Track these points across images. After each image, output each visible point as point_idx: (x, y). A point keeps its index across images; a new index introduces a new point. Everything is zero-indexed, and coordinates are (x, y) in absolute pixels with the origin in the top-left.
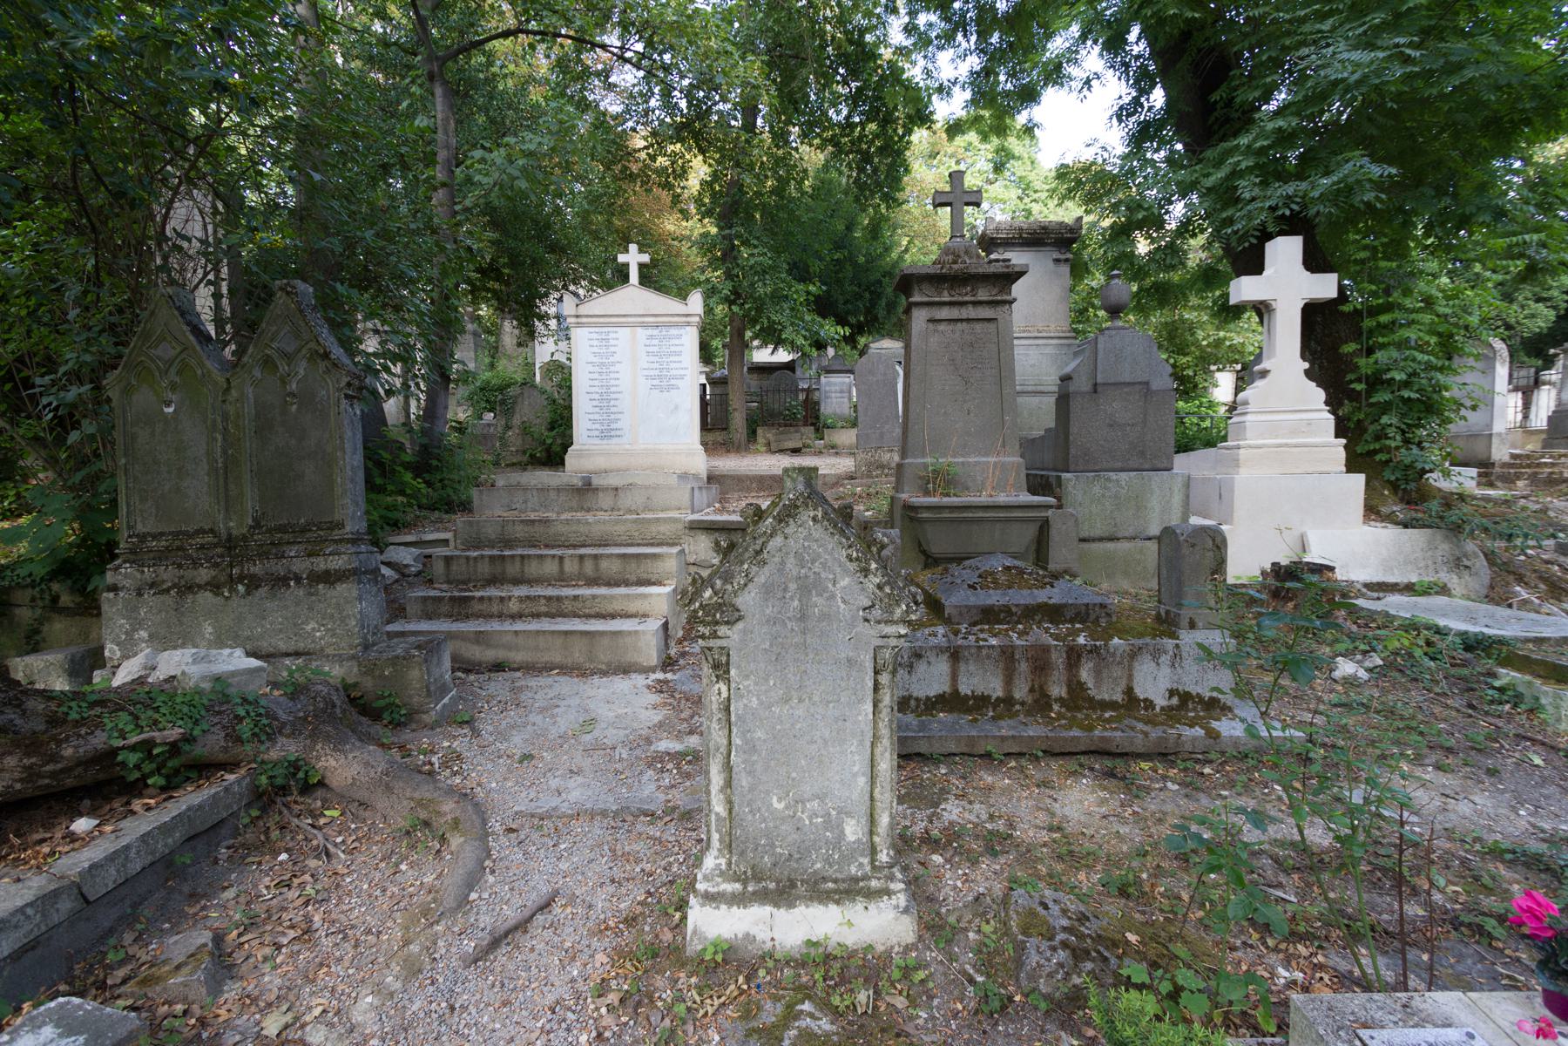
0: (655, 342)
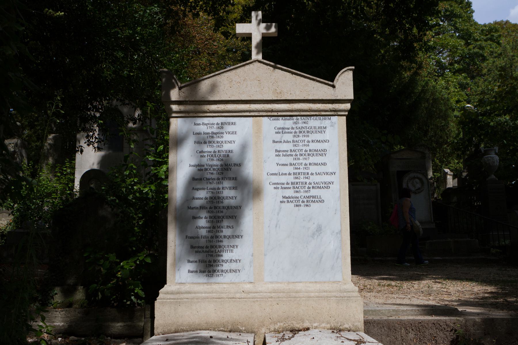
0: (289, 137)
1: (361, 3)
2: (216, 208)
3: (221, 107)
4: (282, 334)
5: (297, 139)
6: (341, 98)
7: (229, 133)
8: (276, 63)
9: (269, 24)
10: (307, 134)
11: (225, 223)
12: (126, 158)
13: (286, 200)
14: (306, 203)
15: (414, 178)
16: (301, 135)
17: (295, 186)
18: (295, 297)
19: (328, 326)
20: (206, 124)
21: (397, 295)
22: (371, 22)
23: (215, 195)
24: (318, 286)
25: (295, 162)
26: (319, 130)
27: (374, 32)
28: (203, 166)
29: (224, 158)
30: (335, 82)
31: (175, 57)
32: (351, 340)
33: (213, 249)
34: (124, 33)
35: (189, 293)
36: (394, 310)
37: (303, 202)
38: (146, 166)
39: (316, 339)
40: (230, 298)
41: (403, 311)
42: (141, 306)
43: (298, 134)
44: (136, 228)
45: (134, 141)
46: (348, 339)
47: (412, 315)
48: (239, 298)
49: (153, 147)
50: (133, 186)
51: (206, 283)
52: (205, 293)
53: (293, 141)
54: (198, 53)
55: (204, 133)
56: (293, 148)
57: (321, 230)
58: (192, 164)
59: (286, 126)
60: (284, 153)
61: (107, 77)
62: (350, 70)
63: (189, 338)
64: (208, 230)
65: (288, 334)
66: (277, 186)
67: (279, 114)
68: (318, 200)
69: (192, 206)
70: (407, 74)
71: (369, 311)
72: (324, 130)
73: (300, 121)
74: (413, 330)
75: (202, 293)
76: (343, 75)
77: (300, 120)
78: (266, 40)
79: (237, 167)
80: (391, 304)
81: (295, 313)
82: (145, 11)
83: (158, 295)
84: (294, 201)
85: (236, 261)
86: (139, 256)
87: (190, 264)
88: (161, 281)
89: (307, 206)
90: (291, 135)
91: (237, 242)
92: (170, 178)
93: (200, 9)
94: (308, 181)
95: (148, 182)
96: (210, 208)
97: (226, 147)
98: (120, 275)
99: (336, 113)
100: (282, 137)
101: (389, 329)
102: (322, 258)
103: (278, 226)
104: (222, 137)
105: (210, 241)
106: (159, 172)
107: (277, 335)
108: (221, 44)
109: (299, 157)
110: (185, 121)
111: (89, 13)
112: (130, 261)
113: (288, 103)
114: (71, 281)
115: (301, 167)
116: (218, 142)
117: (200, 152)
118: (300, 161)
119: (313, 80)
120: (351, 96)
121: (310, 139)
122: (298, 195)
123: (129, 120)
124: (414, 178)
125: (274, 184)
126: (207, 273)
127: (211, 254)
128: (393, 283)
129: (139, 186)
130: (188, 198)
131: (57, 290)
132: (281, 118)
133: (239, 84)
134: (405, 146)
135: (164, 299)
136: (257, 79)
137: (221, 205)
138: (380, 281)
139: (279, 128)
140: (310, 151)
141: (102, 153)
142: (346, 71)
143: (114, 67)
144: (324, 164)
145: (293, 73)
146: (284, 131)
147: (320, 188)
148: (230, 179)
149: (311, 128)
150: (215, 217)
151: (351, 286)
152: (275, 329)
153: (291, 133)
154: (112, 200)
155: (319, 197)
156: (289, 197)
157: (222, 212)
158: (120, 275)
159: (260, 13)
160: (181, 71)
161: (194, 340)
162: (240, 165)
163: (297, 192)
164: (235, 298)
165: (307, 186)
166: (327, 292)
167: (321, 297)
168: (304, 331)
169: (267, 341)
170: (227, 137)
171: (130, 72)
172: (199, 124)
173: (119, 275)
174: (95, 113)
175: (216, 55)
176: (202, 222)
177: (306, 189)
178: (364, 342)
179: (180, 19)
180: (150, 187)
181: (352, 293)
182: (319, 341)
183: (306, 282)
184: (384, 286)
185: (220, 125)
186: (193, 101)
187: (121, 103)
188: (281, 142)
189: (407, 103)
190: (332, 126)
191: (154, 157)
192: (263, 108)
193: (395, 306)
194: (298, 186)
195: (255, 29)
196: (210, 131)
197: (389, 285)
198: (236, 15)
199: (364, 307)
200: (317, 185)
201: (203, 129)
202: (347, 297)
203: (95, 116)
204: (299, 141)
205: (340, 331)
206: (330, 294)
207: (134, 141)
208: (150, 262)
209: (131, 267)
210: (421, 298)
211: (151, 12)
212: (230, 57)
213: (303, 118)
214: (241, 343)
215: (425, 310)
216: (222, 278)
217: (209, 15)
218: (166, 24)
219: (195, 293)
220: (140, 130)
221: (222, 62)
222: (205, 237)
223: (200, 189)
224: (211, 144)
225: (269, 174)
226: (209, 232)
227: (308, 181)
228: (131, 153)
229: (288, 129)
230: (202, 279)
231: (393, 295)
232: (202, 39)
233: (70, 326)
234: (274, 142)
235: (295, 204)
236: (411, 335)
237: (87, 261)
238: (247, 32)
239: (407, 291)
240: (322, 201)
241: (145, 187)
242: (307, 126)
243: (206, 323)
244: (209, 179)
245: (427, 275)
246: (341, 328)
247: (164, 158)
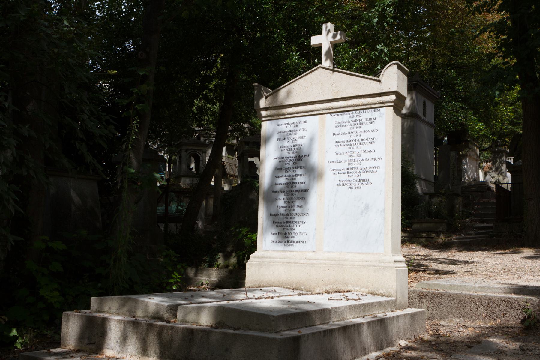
0: (346, 129)
2: (291, 191)
5: (352, 131)
7: (302, 130)
11: (297, 203)
13: (341, 183)
14: (357, 186)
16: (355, 127)
18: (342, 265)
20: (286, 124)
23: (291, 181)
25: (350, 150)
26: (370, 121)
28: (283, 158)
30: (380, 77)
33: (288, 224)
35: (269, 258)
37: (355, 184)
53: (349, 133)
55: (284, 132)
58: (276, 157)
59: (344, 120)
60: (342, 144)
62: (394, 64)
66: (335, 172)
67: (338, 110)
73: (355, 115)
79: (306, 158)
85: (303, 234)
88: (253, 248)
89: (358, 188)
90: (348, 127)
91: (304, 218)
94: (359, 166)
96: (287, 191)
97: (299, 142)
99: (383, 105)
104: (297, 133)
109: (353, 146)
114: (229, 249)
115: (355, 155)
125: (333, 170)
130: (273, 184)
131: (220, 255)
132: (340, 114)
137: (294, 189)
139: (339, 123)
142: (390, 66)
144: (373, 151)
147: (368, 172)
148: (301, 167)
149: (364, 120)
153: (348, 125)
156: (344, 181)
162: (307, 156)
163: (351, 176)
165: (358, 171)
167: (363, 266)
170: (300, 134)
172: (281, 125)
176: (281, 203)
177: (358, 174)
188: (339, 134)
190: (380, 116)
194: (351, 171)
196: (288, 129)
201: (284, 128)
215: (511, 289)
219: (273, 258)
226: (286, 210)
227: (359, 166)
230: (280, 247)
233: (220, 281)
234: (334, 134)
236: (481, 310)
240: (370, 184)
246: (377, 292)
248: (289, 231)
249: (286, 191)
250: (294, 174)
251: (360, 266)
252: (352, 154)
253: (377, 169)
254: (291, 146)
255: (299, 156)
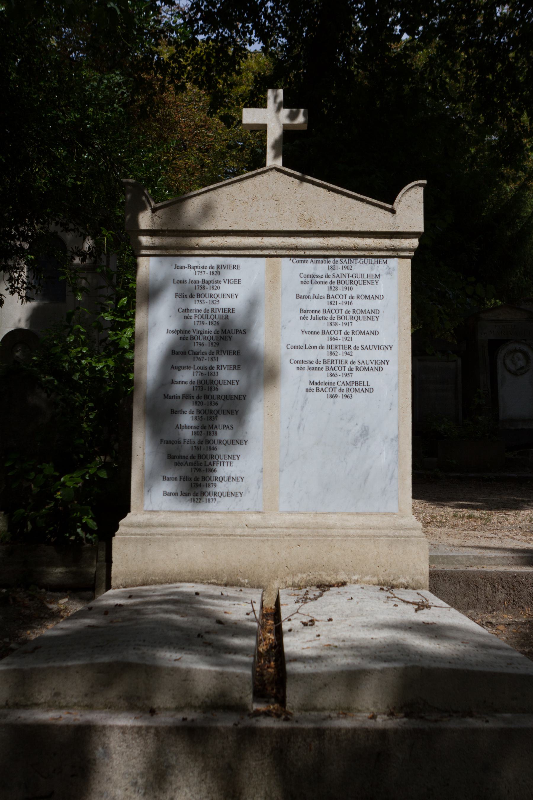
0: (322, 290)
1: (441, 72)
2: (206, 397)
3: (218, 241)
4: (304, 590)
5: (334, 293)
6: (405, 230)
7: (229, 281)
8: (304, 172)
9: (294, 110)
10: (350, 286)
11: (222, 420)
12: (69, 316)
13: (314, 387)
14: (345, 393)
15: (516, 351)
16: (340, 286)
17: (330, 366)
18: (325, 536)
19: (375, 580)
20: (194, 268)
21: (482, 533)
22: (455, 102)
24: (361, 520)
25: (330, 328)
27: (460, 120)
28: (188, 332)
29: (220, 321)
30: (395, 204)
31: (147, 157)
32: (408, 602)
33: (201, 461)
34: (66, 118)
36: (475, 557)
37: (341, 390)
38: (100, 328)
39: (355, 600)
40: (227, 535)
41: (490, 558)
42: (92, 543)
43: (336, 285)
44: (85, 425)
45: (82, 290)
46: (404, 601)
47: (503, 565)
48: (240, 536)
49: (111, 299)
50: (79, 359)
51: (190, 512)
52: (189, 526)
53: (328, 296)
54: (183, 147)
55: (191, 282)
56: (327, 308)
57: (367, 434)
58: (172, 328)
59: (318, 273)
60: (314, 315)
61: (40, 187)
62: (420, 185)
63: (164, 595)
64: (194, 430)
65: (314, 592)
66: (301, 365)
67: (308, 253)
68: (364, 388)
69: (171, 394)
70: (510, 188)
71: (437, 557)
72: (377, 279)
73: (340, 265)
74: (503, 587)
75: (184, 527)
76: (409, 193)
77: (340, 263)
78: (289, 135)
79: (240, 336)
80: (472, 547)
81: (325, 559)
82: (100, 82)
83: (117, 528)
84: (327, 390)
85: (236, 479)
86: (89, 468)
87: (166, 482)
88: (124, 508)
89: (347, 396)
90: (325, 287)
91: (239, 450)
92: (136, 349)
93: (187, 78)
94: (349, 358)
95: (103, 353)
96: (199, 397)
97: (225, 303)
98: (60, 495)
99: (395, 254)
100: (311, 289)
101: (468, 585)
102: (367, 477)
103: (302, 427)
104: (218, 288)
105: (197, 448)
106: (120, 339)
107: (297, 592)
108: (219, 134)
110: (161, 262)
111: (12, 86)
112: (74, 475)
113: (321, 237)
116: (211, 296)
117: (184, 311)
118: (338, 328)
119: (362, 200)
120: (420, 228)
121: (354, 294)
122: (333, 380)
123: (74, 255)
124: (516, 351)
125: (297, 362)
126: (192, 497)
127: (199, 467)
128: (477, 513)
129: (89, 360)
130: (166, 380)
132: (309, 260)
133: (245, 205)
134: (502, 301)
135: (126, 534)
136: (272, 197)
137: (215, 393)
138: (456, 510)
139: (307, 276)
140: (354, 311)
141: (33, 304)
142: (413, 187)
143: (51, 171)
144: (375, 333)
145: (330, 189)
146: (314, 280)
147: (367, 369)
148: (229, 353)
150: (205, 412)
151: (411, 520)
152: (294, 583)
154: (48, 381)
155: (365, 384)
156: (320, 383)
157: (216, 404)
158: (60, 495)
159: (281, 92)
160: (157, 180)
161: (172, 597)
162: (244, 332)
164: (235, 535)
165: (348, 366)
166: (374, 529)
167: (365, 536)
168: (338, 586)
169: (282, 601)
170: (225, 288)
171: (76, 179)
172: (182, 267)
173: (58, 495)
174: (23, 243)
175: (211, 151)
176: (187, 419)
177: (347, 371)
178: (428, 607)
179: (155, 94)
180: (106, 362)
181: (412, 531)
182: (360, 604)
183: (343, 513)
184: (462, 517)
185: (215, 270)
186: (174, 231)
187: (62, 229)
188: (308, 297)
189: (509, 234)
190: (388, 273)
191: (113, 315)
192: (282, 244)
193: (478, 551)
194: (333, 366)
195: (271, 118)
196: (199, 278)
197: (470, 517)
198: (243, 87)
199: (430, 550)
200: (363, 365)
201: (189, 274)
202: (405, 537)
203: (22, 248)
204: (338, 297)
205: (393, 587)
206: (378, 531)
207: (82, 290)
208: (106, 477)
209: (77, 484)
210: (518, 537)
211: (110, 82)
212: (233, 156)
213: (344, 260)
214: (241, 603)
215: (522, 558)
216: (214, 504)
217: (200, 88)
218: (133, 101)
219: (173, 526)
220: (91, 269)
221: (221, 163)
222: (190, 442)
223: (183, 368)
224: (200, 299)
225: (289, 347)
226: (196, 433)
227: (349, 358)
228: (78, 308)
229: (321, 277)
230: (186, 506)
231: (476, 532)
232: (190, 126)
234: (298, 296)
235: (329, 393)
236: (501, 595)
237: (10, 474)
238: (260, 122)
239: (497, 526)
241: (99, 362)
242: (351, 272)
243: (190, 572)
244: (197, 353)
245: (529, 501)
246: (394, 583)
247: (127, 317)
248: (205, 474)
249: (195, 395)
250: (215, 364)
251: (359, 536)
252: (333, 336)
253: (383, 366)
254: (206, 311)
255: (224, 331)
